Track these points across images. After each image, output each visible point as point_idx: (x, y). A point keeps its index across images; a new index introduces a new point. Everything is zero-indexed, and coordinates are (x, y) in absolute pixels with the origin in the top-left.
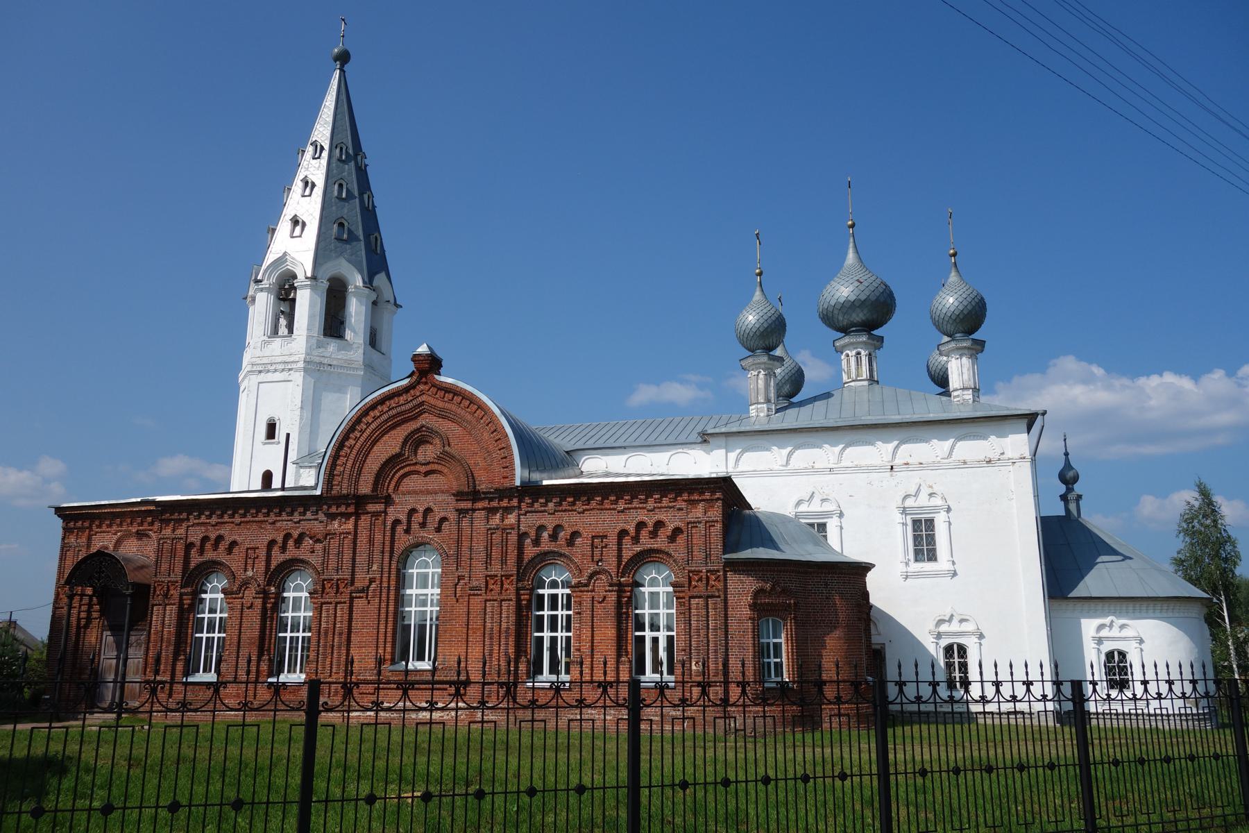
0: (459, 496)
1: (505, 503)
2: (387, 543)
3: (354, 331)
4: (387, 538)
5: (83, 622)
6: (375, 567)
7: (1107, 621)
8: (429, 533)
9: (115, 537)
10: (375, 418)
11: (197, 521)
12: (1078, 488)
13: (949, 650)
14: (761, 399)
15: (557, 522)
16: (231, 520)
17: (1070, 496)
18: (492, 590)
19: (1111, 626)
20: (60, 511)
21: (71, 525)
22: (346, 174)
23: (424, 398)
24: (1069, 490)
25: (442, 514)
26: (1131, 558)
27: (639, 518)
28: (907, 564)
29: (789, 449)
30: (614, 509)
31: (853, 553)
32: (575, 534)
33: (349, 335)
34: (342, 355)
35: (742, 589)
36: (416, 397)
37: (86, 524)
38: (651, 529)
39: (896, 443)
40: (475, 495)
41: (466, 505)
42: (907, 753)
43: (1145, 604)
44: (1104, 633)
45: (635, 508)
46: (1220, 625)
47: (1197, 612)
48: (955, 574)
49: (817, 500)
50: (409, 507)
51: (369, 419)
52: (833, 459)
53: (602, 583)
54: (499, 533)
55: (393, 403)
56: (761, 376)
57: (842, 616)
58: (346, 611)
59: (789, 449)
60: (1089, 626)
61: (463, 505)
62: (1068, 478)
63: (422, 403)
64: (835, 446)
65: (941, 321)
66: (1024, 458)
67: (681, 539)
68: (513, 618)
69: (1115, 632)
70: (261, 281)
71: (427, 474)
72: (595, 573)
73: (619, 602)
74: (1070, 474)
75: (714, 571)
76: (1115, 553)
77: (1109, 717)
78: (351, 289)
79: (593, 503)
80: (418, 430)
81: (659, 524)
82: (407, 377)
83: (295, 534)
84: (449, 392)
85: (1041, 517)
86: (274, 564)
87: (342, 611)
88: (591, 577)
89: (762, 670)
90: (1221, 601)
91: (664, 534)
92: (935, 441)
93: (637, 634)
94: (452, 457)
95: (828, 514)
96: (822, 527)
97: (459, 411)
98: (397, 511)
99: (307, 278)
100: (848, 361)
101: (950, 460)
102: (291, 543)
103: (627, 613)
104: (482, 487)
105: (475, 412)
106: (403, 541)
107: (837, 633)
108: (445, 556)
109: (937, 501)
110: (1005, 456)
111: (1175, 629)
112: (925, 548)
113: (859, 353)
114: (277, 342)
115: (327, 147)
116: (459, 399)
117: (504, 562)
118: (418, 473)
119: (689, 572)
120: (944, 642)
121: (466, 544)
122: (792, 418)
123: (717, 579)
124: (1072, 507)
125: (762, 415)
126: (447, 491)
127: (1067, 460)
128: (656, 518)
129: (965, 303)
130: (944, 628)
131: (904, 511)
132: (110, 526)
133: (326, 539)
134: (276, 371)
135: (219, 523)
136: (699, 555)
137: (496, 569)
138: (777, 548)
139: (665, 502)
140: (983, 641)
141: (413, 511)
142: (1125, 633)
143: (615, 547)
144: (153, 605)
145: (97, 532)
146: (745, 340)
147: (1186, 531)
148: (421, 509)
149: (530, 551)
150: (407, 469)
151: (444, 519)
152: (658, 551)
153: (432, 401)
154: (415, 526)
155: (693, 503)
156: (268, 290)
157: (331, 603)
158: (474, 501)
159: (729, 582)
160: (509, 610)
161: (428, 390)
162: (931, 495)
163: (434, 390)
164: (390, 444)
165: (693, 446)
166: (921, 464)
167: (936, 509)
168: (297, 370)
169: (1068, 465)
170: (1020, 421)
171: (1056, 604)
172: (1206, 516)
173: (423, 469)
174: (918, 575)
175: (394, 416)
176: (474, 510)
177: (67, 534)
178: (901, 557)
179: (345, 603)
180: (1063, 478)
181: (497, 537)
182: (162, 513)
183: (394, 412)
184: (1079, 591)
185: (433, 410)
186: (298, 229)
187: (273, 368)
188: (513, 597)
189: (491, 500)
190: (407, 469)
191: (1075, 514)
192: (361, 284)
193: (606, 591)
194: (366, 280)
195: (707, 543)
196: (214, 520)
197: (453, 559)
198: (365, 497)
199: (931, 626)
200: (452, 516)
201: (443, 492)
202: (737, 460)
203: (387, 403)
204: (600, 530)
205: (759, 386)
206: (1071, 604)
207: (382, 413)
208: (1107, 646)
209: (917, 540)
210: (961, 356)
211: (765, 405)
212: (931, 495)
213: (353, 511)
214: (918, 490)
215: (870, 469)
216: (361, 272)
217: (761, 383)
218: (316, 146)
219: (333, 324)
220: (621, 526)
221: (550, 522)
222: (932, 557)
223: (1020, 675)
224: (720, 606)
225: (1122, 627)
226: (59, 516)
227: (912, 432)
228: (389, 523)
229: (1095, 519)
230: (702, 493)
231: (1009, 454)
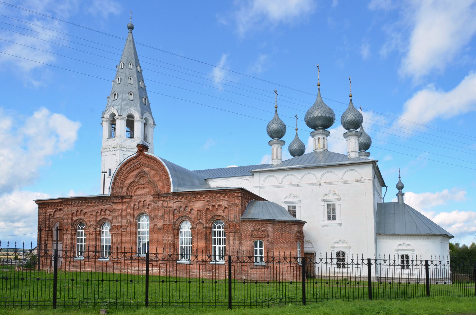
5: (46, 239)
6: (129, 221)
8: (145, 209)
9: (54, 211)
11: (74, 205)
16: (102, 204)
20: (37, 202)
21: (41, 206)
23: (142, 160)
25: (149, 203)
30: (204, 200)
36: (139, 160)
37: (45, 206)
38: (80, 213)
41: (157, 199)
42: (170, 286)
43: (425, 237)
44: (400, 248)
50: (139, 200)
51: (124, 168)
55: (131, 163)
58: (120, 236)
61: (156, 199)
63: (141, 163)
66: (370, 179)
67: (226, 211)
71: (144, 188)
75: (238, 223)
77: (399, 279)
82: (136, 153)
83: (104, 210)
86: (98, 220)
87: (119, 237)
98: (135, 201)
101: (342, 181)
102: (103, 212)
105: (158, 165)
106: (137, 212)
108: (150, 217)
110: (362, 179)
112: (331, 215)
114: (111, 140)
118: (141, 188)
119: (230, 223)
126: (151, 194)
127: (400, 180)
128: (219, 204)
132: (51, 207)
133: (113, 211)
135: (81, 206)
143: (205, 214)
144: (64, 234)
145: (48, 209)
146: (271, 134)
148: (142, 201)
149: (177, 216)
150: (137, 186)
153: (145, 162)
157: (115, 233)
160: (171, 236)
161: (143, 158)
163: (145, 157)
164: (131, 178)
166: (331, 182)
169: (400, 182)
170: (369, 164)
173: (143, 186)
177: (40, 210)
179: (120, 233)
182: (64, 202)
183: (132, 166)
185: (145, 165)
189: (164, 197)
190: (137, 186)
193: (202, 230)
196: (79, 205)
197: (153, 219)
198: (124, 196)
200: (152, 203)
201: (149, 195)
204: (200, 208)
207: (129, 166)
213: (121, 201)
220: (207, 207)
221: (184, 205)
222: (334, 218)
226: (37, 203)
228: (132, 206)
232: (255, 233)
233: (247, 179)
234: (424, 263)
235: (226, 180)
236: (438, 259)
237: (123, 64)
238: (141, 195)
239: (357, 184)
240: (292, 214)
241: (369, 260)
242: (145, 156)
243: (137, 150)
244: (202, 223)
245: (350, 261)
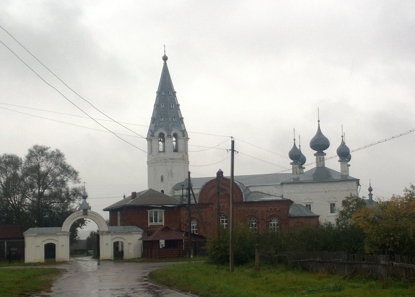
12: (372, 192)
31: (317, 214)
232: (296, 224)
233: (276, 187)
237: (164, 92)
240: (308, 207)
244: (264, 219)
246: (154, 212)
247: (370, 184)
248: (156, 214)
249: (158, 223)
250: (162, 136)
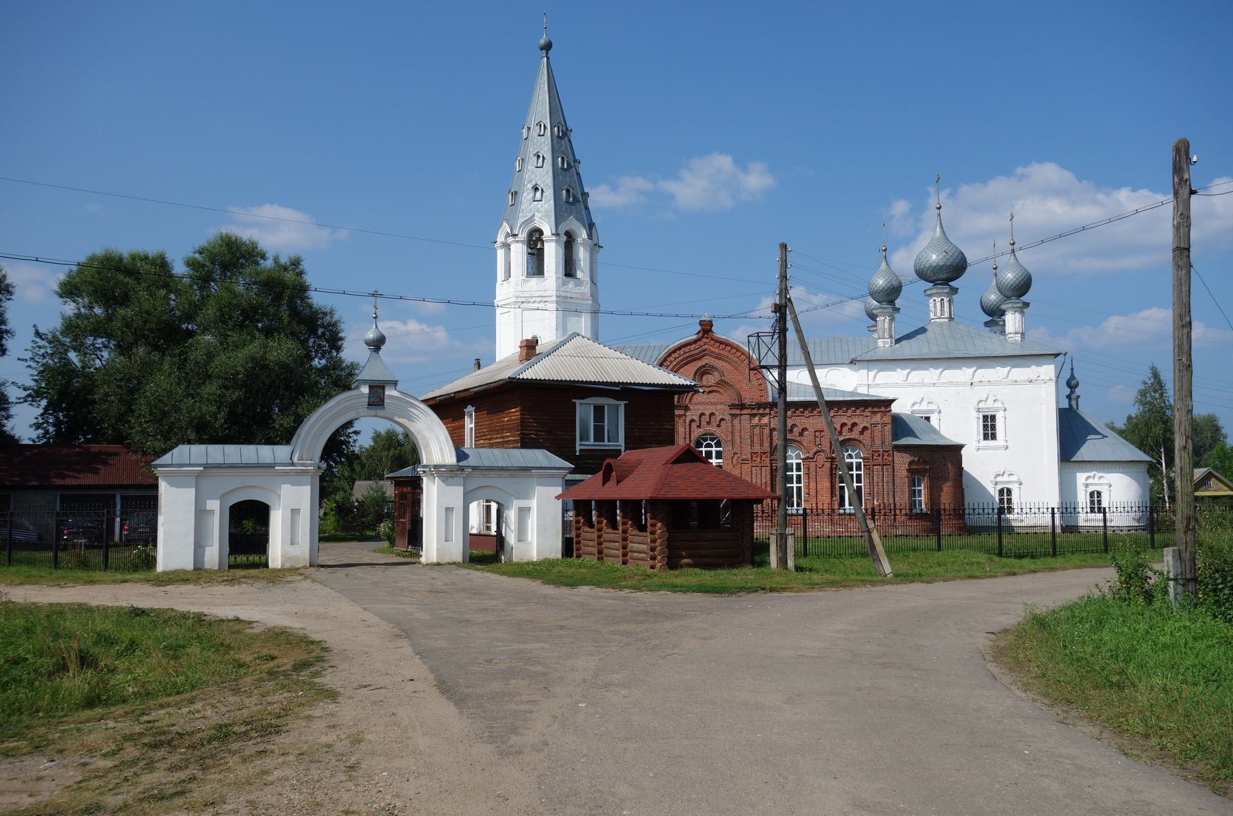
0: (733, 406)
1: (761, 411)
2: (688, 433)
3: (582, 271)
4: (687, 430)
7: (1092, 474)
8: (712, 427)
10: (675, 358)
12: (1078, 391)
13: (1001, 492)
14: (887, 336)
15: (793, 423)
17: (1072, 396)
18: (755, 461)
19: (1094, 477)
22: (563, 148)
23: (706, 347)
24: (1072, 392)
25: (721, 417)
26: (1107, 437)
27: (843, 421)
28: (979, 442)
29: (908, 370)
31: (956, 440)
32: (804, 429)
33: (579, 274)
34: (578, 290)
35: (902, 462)
36: (701, 346)
39: (975, 368)
40: (742, 406)
44: (1089, 481)
45: (840, 415)
46: (1159, 469)
47: (1144, 468)
48: (1007, 448)
49: (925, 403)
50: (700, 412)
52: (935, 378)
53: (821, 458)
54: (758, 428)
55: (687, 349)
56: (887, 320)
57: (951, 475)
59: (908, 370)
60: (1081, 477)
61: (734, 412)
62: (1072, 385)
63: (705, 350)
64: (937, 369)
65: (1003, 289)
67: (867, 433)
68: (769, 477)
69: (1096, 481)
70: (517, 235)
72: (818, 452)
73: (831, 468)
74: (1074, 382)
76: (1099, 434)
78: (579, 240)
79: (815, 412)
80: (704, 366)
81: (854, 424)
84: (717, 342)
85: (1059, 409)
88: (815, 454)
89: (913, 504)
90: (1161, 452)
91: (858, 429)
92: (999, 368)
93: (841, 485)
94: (727, 383)
95: (932, 411)
96: (928, 419)
97: (729, 355)
99: (552, 234)
100: (935, 304)
103: (835, 474)
104: (747, 401)
107: (949, 484)
109: (998, 405)
111: (1129, 479)
112: (990, 432)
113: (942, 300)
115: (548, 126)
116: (729, 348)
117: (761, 445)
120: (999, 487)
121: (737, 434)
122: (908, 348)
123: (888, 455)
124: (1074, 403)
125: (887, 346)
129: (1020, 279)
130: (999, 479)
131: (978, 410)
134: (535, 302)
136: (878, 442)
137: (757, 448)
138: (916, 437)
139: (858, 412)
140: (1021, 486)
141: (702, 414)
142: (1102, 481)
147: (1141, 402)
148: (708, 414)
151: (722, 420)
152: (853, 440)
153: (712, 349)
154: (704, 423)
155: (874, 413)
156: (522, 242)
158: (741, 409)
159: (895, 457)
162: (995, 401)
163: (713, 342)
165: (843, 365)
167: (997, 410)
168: (551, 302)
169: (1072, 377)
171: (1064, 464)
172: (1155, 391)
173: (707, 390)
174: (985, 448)
175: (687, 357)
176: (741, 415)
178: (975, 437)
180: (1069, 384)
181: (757, 431)
183: (688, 355)
184: (1078, 457)
185: (712, 354)
186: (538, 194)
187: (532, 300)
188: (769, 465)
189: (753, 409)
191: (1075, 408)
192: (586, 237)
194: (589, 233)
195: (883, 435)
199: (992, 478)
200: (728, 418)
202: (875, 377)
203: (683, 349)
204: (819, 427)
205: (885, 327)
206: (1072, 465)
208: (1091, 489)
209: (985, 427)
210: (1015, 312)
211: (889, 340)
212: (995, 401)
214: (988, 398)
215: (957, 384)
216: (585, 228)
217: (886, 326)
218: (540, 125)
219: (569, 270)
222: (994, 437)
223: (991, 507)
224: (890, 470)
225: (1100, 477)
227: (985, 362)
229: (1086, 411)
230: (880, 408)
231: (1043, 377)
234: (1050, 510)
235: (798, 371)
236: (1028, 507)
238: (703, 403)
239: (1031, 386)
241: (1053, 509)
242: (712, 339)
243: (699, 328)
244: (823, 451)
245: (1080, 510)
246: (594, 406)
247: (1072, 369)
248: (599, 411)
249: (606, 442)
250: (362, 490)
